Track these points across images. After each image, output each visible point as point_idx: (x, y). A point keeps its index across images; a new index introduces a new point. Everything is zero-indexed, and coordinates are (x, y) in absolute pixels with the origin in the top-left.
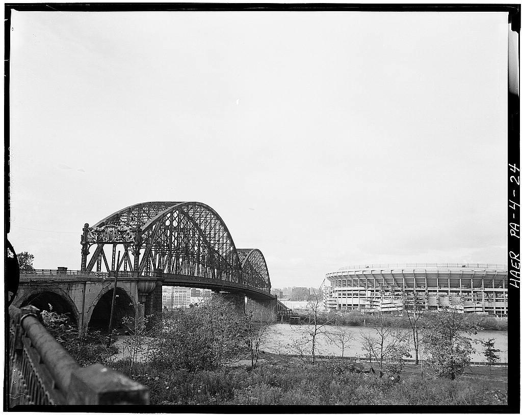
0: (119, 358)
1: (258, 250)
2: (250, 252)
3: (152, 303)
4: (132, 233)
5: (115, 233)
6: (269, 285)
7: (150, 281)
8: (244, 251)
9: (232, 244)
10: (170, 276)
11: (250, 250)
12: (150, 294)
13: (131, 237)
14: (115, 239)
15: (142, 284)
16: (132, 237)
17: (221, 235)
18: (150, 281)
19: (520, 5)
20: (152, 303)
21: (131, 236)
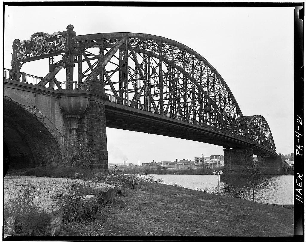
0: (228, 217)
1: (261, 117)
2: (253, 118)
3: (85, 129)
4: (62, 38)
5: (44, 43)
6: (274, 147)
7: (77, 94)
8: (249, 118)
9: (239, 112)
10: (52, 55)
11: (253, 116)
12: (83, 115)
13: (61, 44)
14: (45, 50)
15: (65, 101)
16: (63, 43)
17: (222, 96)
18: (83, 95)
19: (304, 241)
20: (85, 129)
21: (61, 42)
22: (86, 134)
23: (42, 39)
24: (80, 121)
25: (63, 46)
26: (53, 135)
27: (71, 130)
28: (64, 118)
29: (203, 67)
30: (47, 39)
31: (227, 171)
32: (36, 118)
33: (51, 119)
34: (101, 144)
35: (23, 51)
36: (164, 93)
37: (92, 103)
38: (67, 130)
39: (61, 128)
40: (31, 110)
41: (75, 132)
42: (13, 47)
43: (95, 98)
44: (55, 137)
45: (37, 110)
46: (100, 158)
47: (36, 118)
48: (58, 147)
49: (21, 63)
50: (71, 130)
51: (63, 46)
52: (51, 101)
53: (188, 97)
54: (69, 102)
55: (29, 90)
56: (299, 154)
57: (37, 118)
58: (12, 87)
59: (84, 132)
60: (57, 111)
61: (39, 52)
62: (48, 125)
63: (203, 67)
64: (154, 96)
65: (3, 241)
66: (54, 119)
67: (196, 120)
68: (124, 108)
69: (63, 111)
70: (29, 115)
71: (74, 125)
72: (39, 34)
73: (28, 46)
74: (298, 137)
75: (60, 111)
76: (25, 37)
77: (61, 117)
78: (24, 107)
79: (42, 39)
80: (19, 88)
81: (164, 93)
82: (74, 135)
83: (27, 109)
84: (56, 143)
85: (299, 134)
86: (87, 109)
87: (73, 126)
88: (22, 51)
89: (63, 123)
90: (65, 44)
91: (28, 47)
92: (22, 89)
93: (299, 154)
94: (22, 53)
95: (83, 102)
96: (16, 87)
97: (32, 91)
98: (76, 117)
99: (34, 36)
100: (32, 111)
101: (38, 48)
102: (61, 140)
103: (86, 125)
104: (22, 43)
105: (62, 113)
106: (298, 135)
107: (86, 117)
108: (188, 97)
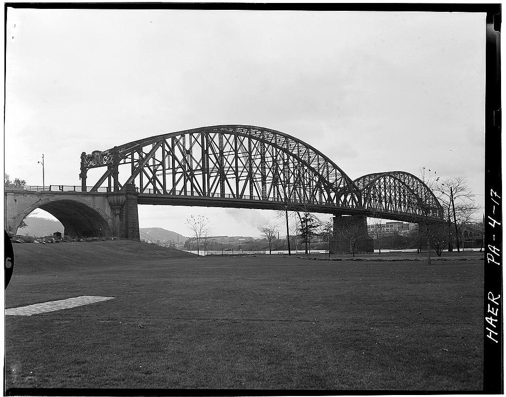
13: (110, 159)
15: (111, 198)
24: (121, 209)
27: (116, 215)
28: (112, 208)
29: (414, 180)
36: (380, 251)
41: (118, 216)
43: (129, 196)
50: (116, 215)
53: (200, 162)
56: (493, 261)
60: (107, 204)
62: (101, 213)
63: (418, 183)
65: (503, 394)
69: (110, 204)
70: (90, 208)
71: (118, 212)
74: (493, 226)
81: (380, 251)
85: (495, 221)
87: (117, 213)
93: (493, 261)
95: (122, 198)
106: (492, 222)
108: (200, 162)
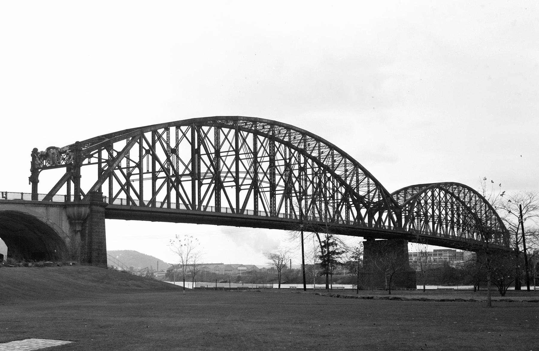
3: (87, 232)
12: (85, 220)
14: (58, 162)
15: (70, 210)
16: (72, 158)
20: (87, 232)
22: (87, 235)
23: (55, 152)
24: (83, 225)
25: (71, 160)
26: (61, 237)
28: (71, 223)
30: (59, 153)
31: (367, 275)
32: (47, 225)
33: (59, 225)
34: (100, 243)
35: (41, 160)
37: (91, 211)
38: (73, 232)
39: (67, 230)
40: (44, 220)
41: (79, 234)
42: (32, 155)
44: (63, 238)
45: (48, 219)
46: (99, 254)
47: (47, 225)
48: (65, 246)
49: (39, 170)
50: (76, 232)
51: (71, 160)
52: (59, 211)
54: (72, 211)
55: (41, 205)
57: (48, 225)
58: (30, 205)
59: (86, 233)
60: (64, 218)
61: (54, 163)
62: (56, 229)
64: (228, 172)
66: (62, 224)
67: (359, 193)
68: (131, 208)
69: (69, 218)
70: (41, 223)
71: (79, 228)
72: (54, 148)
73: (45, 155)
75: (66, 218)
76: (42, 149)
77: (68, 222)
78: (38, 218)
79: (55, 152)
80: (34, 205)
82: (78, 236)
83: (40, 219)
84: (64, 243)
86: (88, 216)
87: (77, 229)
88: (40, 160)
89: (69, 227)
90: (73, 158)
91: (44, 157)
92: (36, 205)
94: (39, 162)
95: (85, 211)
96: (32, 205)
97: (43, 206)
98: (80, 222)
99: (49, 149)
100: (44, 220)
101: (53, 159)
102: (68, 240)
103: (87, 228)
104: (39, 154)
105: (68, 219)
107: (88, 222)
